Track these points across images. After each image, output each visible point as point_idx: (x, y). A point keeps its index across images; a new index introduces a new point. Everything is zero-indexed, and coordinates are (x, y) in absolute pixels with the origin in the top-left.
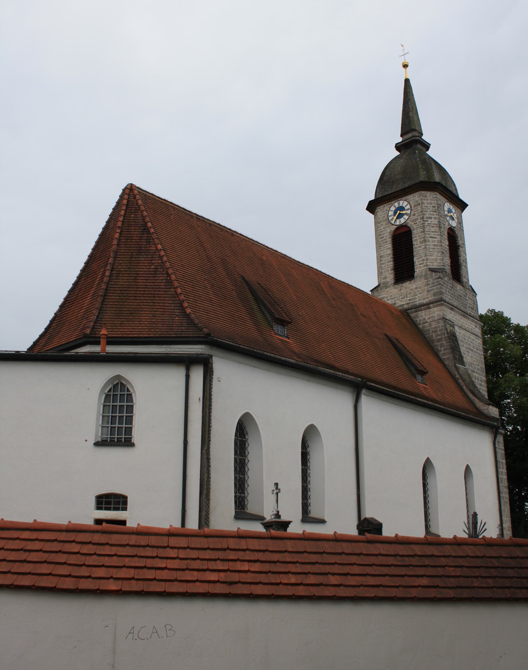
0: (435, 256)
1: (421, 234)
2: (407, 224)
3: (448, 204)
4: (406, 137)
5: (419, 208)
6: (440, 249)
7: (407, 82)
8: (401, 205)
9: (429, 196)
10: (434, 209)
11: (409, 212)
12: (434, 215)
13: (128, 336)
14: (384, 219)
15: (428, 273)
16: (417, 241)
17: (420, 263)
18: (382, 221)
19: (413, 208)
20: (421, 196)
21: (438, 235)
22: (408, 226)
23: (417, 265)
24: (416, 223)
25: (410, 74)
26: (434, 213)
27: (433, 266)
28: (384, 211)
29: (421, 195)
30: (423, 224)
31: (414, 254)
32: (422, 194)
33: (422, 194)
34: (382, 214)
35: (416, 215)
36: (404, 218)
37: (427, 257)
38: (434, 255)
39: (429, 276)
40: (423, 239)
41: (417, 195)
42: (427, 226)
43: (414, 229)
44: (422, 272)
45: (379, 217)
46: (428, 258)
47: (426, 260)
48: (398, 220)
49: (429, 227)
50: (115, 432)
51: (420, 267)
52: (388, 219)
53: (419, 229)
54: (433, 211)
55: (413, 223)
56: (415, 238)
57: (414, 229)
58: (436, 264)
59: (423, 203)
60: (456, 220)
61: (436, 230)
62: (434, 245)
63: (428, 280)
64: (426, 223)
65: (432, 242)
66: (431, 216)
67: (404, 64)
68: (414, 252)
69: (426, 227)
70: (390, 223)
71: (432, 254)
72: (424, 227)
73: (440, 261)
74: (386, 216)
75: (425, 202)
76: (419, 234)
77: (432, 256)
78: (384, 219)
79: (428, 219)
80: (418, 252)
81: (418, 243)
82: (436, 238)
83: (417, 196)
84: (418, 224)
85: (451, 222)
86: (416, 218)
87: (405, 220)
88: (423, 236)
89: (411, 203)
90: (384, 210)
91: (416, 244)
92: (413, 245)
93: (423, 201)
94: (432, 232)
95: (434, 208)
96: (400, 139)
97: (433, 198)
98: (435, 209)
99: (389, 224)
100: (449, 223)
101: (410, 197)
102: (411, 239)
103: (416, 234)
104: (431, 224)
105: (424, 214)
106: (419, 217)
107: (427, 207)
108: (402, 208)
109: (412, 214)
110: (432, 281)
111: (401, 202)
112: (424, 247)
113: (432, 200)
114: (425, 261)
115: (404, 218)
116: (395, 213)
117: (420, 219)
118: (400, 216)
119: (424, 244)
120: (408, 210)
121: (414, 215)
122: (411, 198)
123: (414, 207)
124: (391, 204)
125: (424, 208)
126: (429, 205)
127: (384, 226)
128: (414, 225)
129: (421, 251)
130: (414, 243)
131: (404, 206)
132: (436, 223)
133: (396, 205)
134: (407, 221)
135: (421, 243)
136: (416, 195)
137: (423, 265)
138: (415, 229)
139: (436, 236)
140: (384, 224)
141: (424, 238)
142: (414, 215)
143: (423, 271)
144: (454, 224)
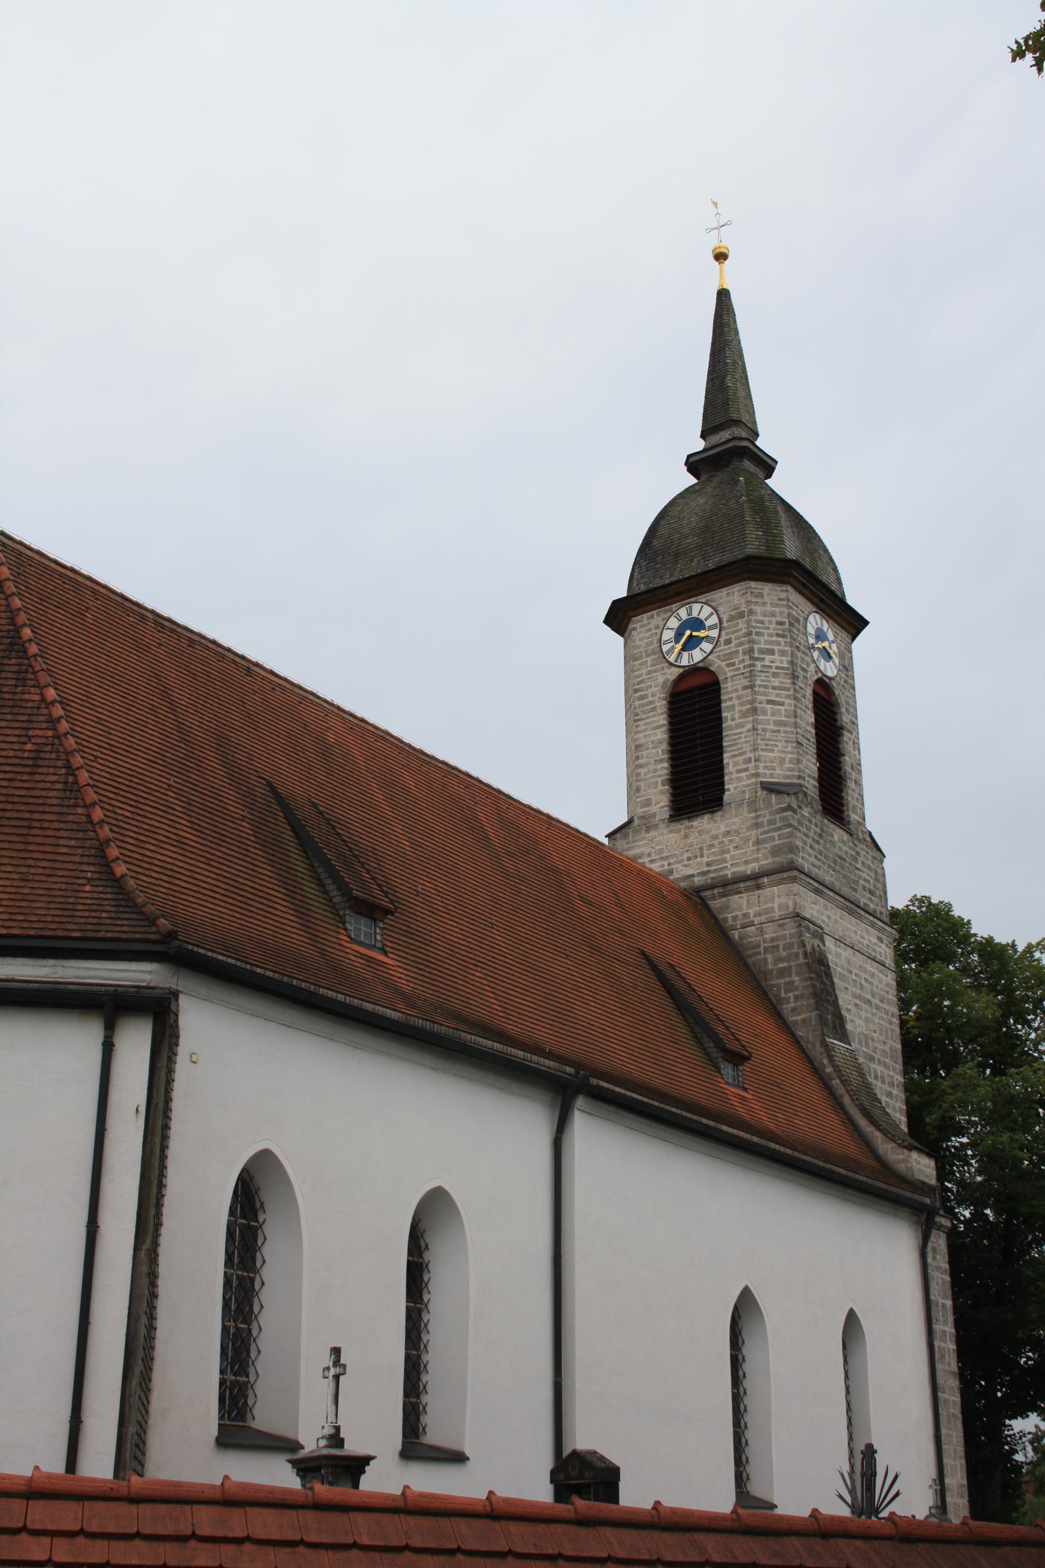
1: (744, 692)
3: (818, 616)
4: (716, 439)
5: (741, 624)
6: (792, 733)
7: (723, 296)
8: (695, 614)
10: (780, 630)
11: (714, 633)
12: (778, 644)
14: (650, 648)
16: (734, 710)
18: (644, 654)
19: (725, 625)
20: (749, 595)
21: (788, 697)
23: (732, 773)
24: (733, 664)
26: (780, 639)
27: (772, 776)
28: (650, 630)
29: (748, 590)
30: (750, 666)
32: (750, 588)
33: (750, 588)
34: (643, 637)
35: (734, 642)
36: (701, 649)
37: (757, 754)
38: (776, 749)
39: (761, 803)
40: (749, 706)
42: (761, 671)
43: (726, 678)
44: (744, 792)
45: (638, 643)
46: (759, 755)
48: (685, 654)
49: (765, 676)
51: (740, 779)
52: (659, 649)
53: (740, 679)
54: (778, 635)
55: (723, 664)
56: (729, 703)
57: (726, 678)
59: (751, 612)
60: (836, 660)
61: (786, 683)
63: (758, 813)
64: (759, 664)
66: (771, 647)
68: (725, 739)
72: (752, 675)
74: (655, 641)
75: (758, 609)
76: (740, 693)
77: (772, 751)
78: (650, 648)
80: (736, 740)
81: (737, 716)
82: (782, 704)
83: (736, 593)
84: (737, 666)
85: (822, 664)
86: (734, 649)
87: (705, 655)
88: (750, 698)
89: (721, 609)
90: (652, 626)
91: (729, 717)
93: (752, 607)
94: (774, 688)
95: (780, 627)
96: (699, 445)
99: (662, 662)
100: (817, 667)
101: (718, 595)
104: (771, 666)
105: (753, 642)
106: (740, 649)
107: (762, 622)
108: (697, 624)
109: (722, 640)
110: (768, 817)
112: (749, 726)
113: (777, 605)
114: (753, 764)
115: (701, 649)
117: (744, 653)
118: (691, 644)
120: (711, 628)
121: (728, 642)
122: (721, 598)
123: (728, 621)
126: (767, 619)
127: (650, 669)
128: (727, 669)
129: (743, 736)
130: (724, 715)
131: (702, 617)
132: (785, 665)
133: (683, 613)
134: (710, 657)
135: (744, 715)
136: (736, 589)
137: (748, 773)
138: (729, 680)
140: (649, 664)
141: (752, 704)
142: (728, 642)
143: (747, 789)
144: (830, 669)
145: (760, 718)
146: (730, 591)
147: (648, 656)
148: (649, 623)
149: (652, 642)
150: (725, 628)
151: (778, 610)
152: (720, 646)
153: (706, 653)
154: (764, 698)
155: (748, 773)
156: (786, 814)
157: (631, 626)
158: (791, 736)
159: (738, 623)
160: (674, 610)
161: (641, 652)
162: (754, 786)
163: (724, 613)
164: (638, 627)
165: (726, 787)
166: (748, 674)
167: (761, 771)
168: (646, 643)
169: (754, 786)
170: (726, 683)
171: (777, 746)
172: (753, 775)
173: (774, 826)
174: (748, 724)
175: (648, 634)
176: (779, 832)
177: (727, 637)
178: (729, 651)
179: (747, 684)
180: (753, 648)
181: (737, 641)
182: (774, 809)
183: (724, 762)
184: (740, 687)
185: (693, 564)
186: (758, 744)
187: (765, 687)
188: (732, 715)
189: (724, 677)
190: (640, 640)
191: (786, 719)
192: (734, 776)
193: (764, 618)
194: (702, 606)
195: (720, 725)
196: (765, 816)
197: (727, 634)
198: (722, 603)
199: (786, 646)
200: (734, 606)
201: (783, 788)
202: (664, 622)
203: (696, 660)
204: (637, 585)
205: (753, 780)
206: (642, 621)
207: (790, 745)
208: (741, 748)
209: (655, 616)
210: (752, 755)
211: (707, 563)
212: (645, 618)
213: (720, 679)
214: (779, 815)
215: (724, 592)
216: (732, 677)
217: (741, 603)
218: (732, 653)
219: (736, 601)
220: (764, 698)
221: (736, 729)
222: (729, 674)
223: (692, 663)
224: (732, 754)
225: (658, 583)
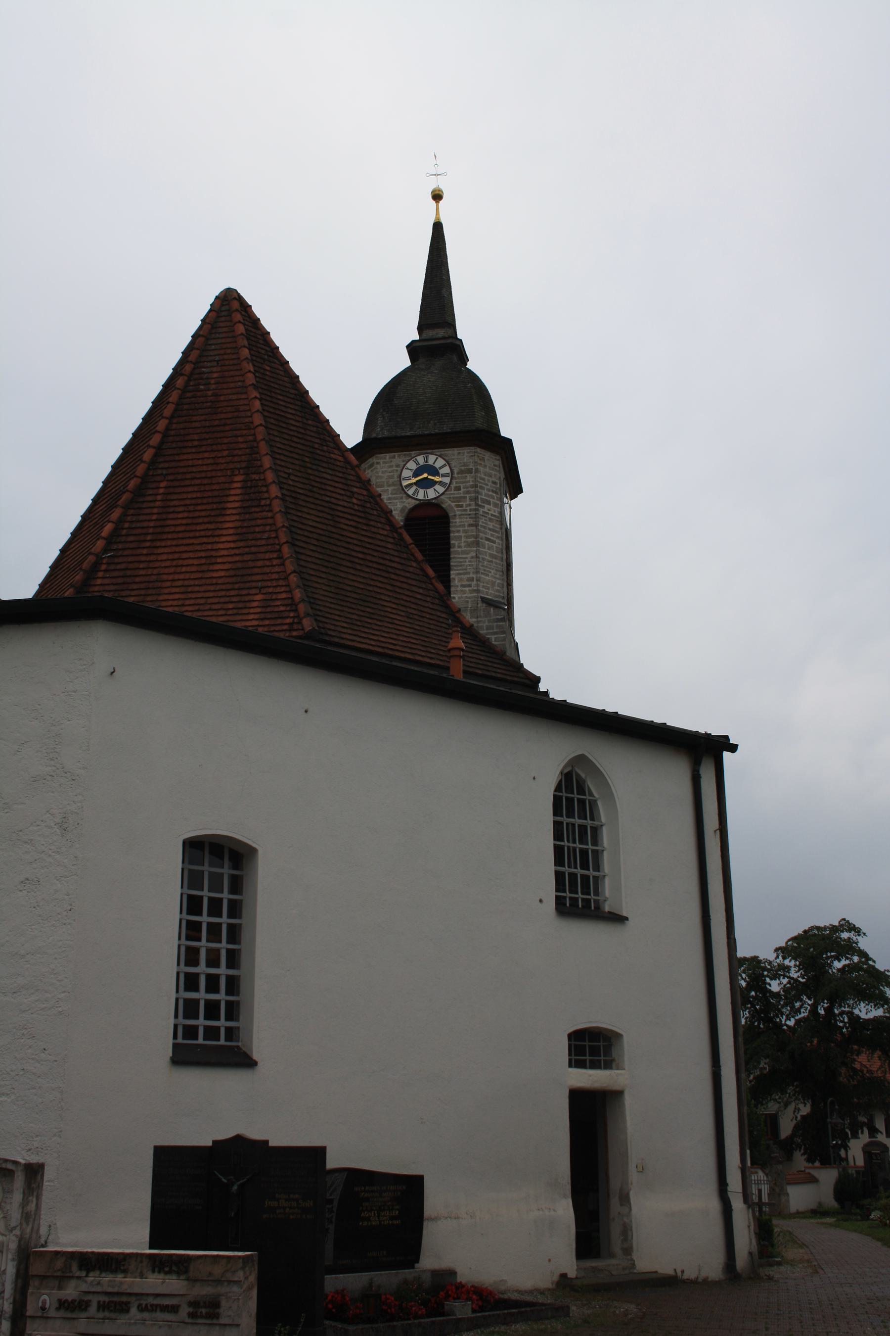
0: (492, 576)
1: (469, 528)
2: (442, 503)
4: (430, 333)
5: (469, 477)
6: (500, 564)
7: (438, 228)
8: (431, 462)
9: (488, 460)
10: (494, 487)
11: (447, 480)
13: (397, 654)
14: (391, 480)
15: (479, 605)
16: (461, 540)
17: (464, 583)
18: (385, 484)
19: (455, 475)
20: (476, 457)
21: (498, 537)
22: (442, 508)
23: (457, 586)
24: (462, 506)
25: (448, 213)
26: (494, 495)
28: (392, 466)
29: (476, 454)
30: (476, 510)
31: (452, 564)
32: (477, 452)
33: (477, 452)
34: (386, 471)
35: (462, 490)
36: (435, 490)
37: (478, 575)
38: (490, 574)
39: (482, 613)
40: (473, 539)
41: (468, 453)
42: (483, 516)
43: (455, 515)
44: (467, 602)
45: (380, 474)
46: (480, 577)
47: (477, 580)
48: (414, 488)
49: (485, 520)
50: (578, 888)
51: (464, 592)
52: (398, 483)
53: (467, 518)
54: (493, 491)
55: (453, 504)
56: (457, 534)
57: (455, 515)
58: (493, 592)
59: (477, 471)
61: (496, 527)
62: (491, 555)
63: (479, 619)
64: (481, 510)
65: (489, 549)
66: (489, 499)
67: (437, 192)
69: (480, 516)
70: (403, 492)
71: (488, 571)
72: (476, 517)
73: (499, 588)
74: (396, 476)
76: (466, 528)
77: (488, 575)
78: (391, 480)
79: (484, 503)
80: (461, 562)
81: (463, 544)
82: (494, 542)
83: (466, 454)
84: (464, 508)
86: (462, 495)
87: (438, 495)
88: (474, 533)
89: (453, 463)
90: (393, 464)
91: (456, 544)
92: (452, 546)
93: (478, 467)
94: (490, 529)
95: (494, 485)
96: (416, 337)
97: (495, 465)
98: (496, 488)
99: (401, 493)
101: (450, 452)
102: (448, 533)
103: (460, 526)
104: (488, 513)
105: (478, 492)
106: (468, 496)
107: (484, 479)
109: (453, 486)
110: (487, 624)
111: (432, 459)
112: (473, 554)
113: (493, 469)
114: (475, 582)
115: (435, 490)
116: (416, 474)
117: (471, 500)
118: (426, 484)
119: (475, 549)
120: (444, 475)
121: (458, 489)
122: (453, 455)
123: (458, 473)
124: (410, 455)
125: (479, 480)
126: (486, 478)
127: (390, 496)
128: (456, 509)
129: (467, 560)
130: (452, 542)
132: (496, 514)
133: (421, 460)
134: (442, 497)
135: (469, 545)
136: (466, 451)
137: (471, 589)
138: (457, 517)
139: (494, 539)
140: (390, 492)
141: (476, 538)
142: (458, 489)
143: (469, 600)
145: (481, 549)
146: (461, 451)
147: (389, 486)
148: (391, 461)
149: (392, 477)
150: (456, 478)
151: (493, 473)
152: (451, 490)
153: (439, 493)
154: (484, 536)
155: (471, 589)
156: (501, 623)
157: (373, 460)
158: (499, 566)
159: (466, 476)
160: (413, 455)
161: (384, 482)
162: (476, 599)
163: (455, 467)
164: (381, 463)
165: (452, 596)
166: (473, 516)
167: (481, 589)
168: (388, 476)
169: (476, 599)
170: (455, 519)
171: (491, 572)
172: (474, 591)
173: (491, 631)
174: (472, 553)
175: (390, 469)
176: (496, 636)
177: (458, 485)
178: (458, 496)
179: (472, 522)
180: (478, 497)
181: (465, 490)
182: (492, 618)
183: (451, 577)
184: (466, 524)
185: (430, 425)
186: (479, 568)
187: (484, 527)
188: (459, 543)
189: (453, 514)
190: (383, 472)
191: (497, 554)
192: (459, 588)
193: (484, 477)
194: (437, 458)
195: (449, 549)
196: (484, 622)
197: (456, 483)
198: (453, 459)
199: (497, 500)
200: (464, 463)
201: (497, 604)
202: (404, 463)
203: (430, 497)
204: (380, 431)
205: (475, 594)
206: (385, 458)
207: (498, 573)
208: (466, 569)
209: (396, 457)
210: (474, 576)
211: (442, 426)
212: (388, 457)
213: (450, 515)
214: (496, 624)
215: (456, 451)
216: (460, 515)
217: (470, 462)
218: (461, 497)
219: (465, 459)
220: (484, 536)
221: (462, 554)
222: (458, 513)
223: (427, 499)
224: (457, 572)
225: (400, 433)
